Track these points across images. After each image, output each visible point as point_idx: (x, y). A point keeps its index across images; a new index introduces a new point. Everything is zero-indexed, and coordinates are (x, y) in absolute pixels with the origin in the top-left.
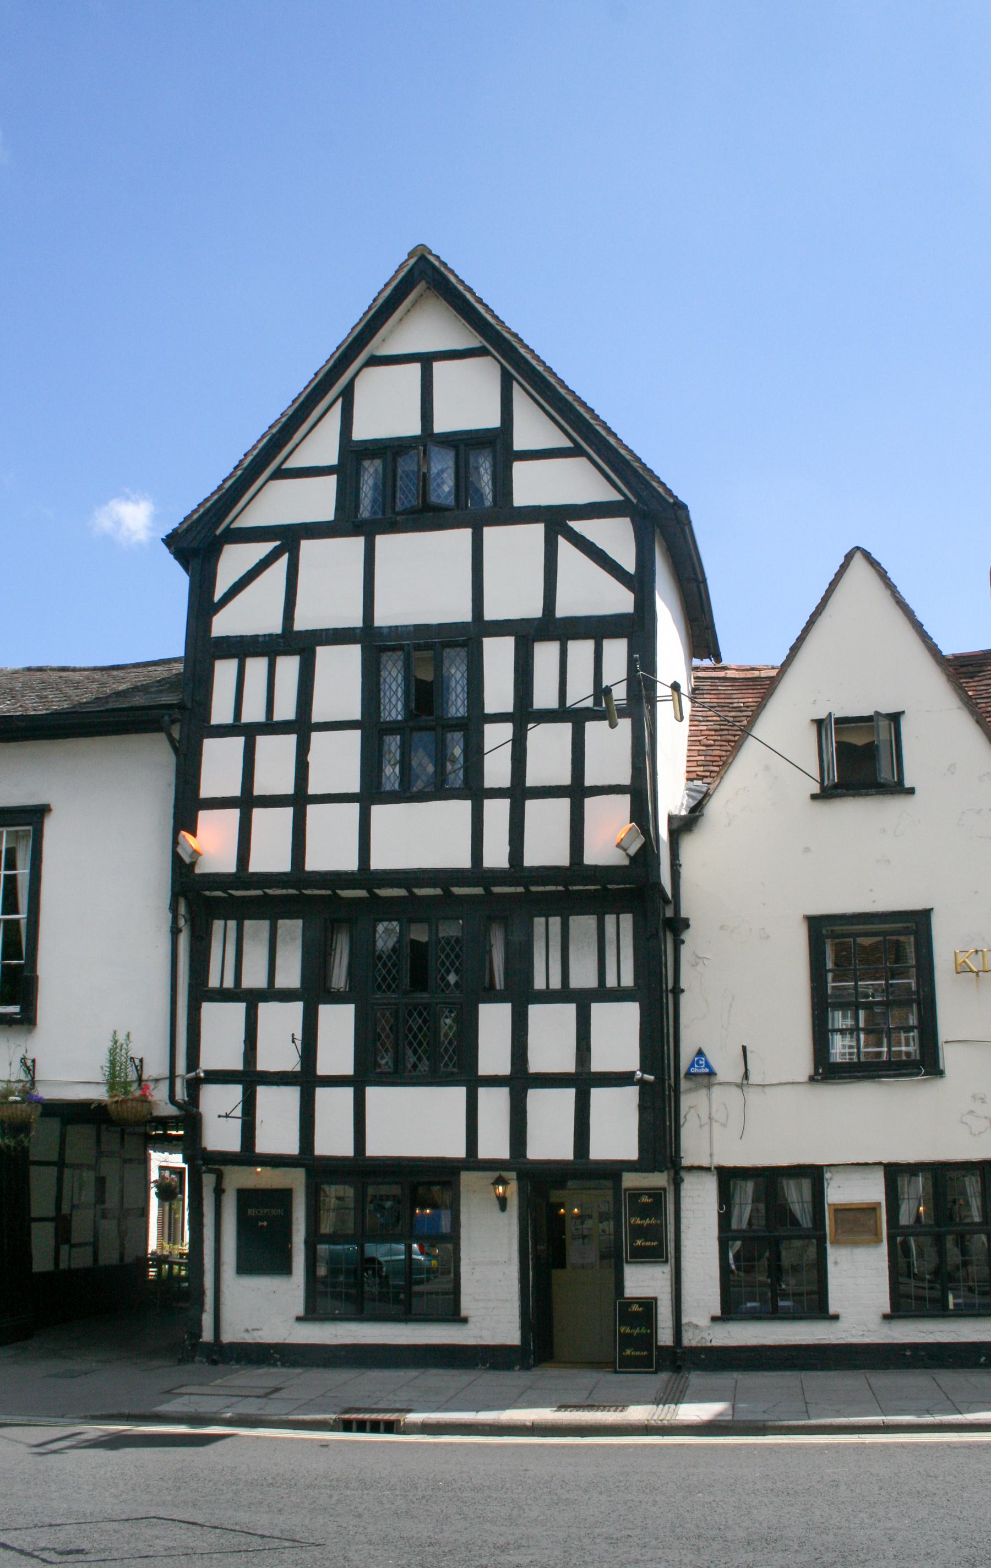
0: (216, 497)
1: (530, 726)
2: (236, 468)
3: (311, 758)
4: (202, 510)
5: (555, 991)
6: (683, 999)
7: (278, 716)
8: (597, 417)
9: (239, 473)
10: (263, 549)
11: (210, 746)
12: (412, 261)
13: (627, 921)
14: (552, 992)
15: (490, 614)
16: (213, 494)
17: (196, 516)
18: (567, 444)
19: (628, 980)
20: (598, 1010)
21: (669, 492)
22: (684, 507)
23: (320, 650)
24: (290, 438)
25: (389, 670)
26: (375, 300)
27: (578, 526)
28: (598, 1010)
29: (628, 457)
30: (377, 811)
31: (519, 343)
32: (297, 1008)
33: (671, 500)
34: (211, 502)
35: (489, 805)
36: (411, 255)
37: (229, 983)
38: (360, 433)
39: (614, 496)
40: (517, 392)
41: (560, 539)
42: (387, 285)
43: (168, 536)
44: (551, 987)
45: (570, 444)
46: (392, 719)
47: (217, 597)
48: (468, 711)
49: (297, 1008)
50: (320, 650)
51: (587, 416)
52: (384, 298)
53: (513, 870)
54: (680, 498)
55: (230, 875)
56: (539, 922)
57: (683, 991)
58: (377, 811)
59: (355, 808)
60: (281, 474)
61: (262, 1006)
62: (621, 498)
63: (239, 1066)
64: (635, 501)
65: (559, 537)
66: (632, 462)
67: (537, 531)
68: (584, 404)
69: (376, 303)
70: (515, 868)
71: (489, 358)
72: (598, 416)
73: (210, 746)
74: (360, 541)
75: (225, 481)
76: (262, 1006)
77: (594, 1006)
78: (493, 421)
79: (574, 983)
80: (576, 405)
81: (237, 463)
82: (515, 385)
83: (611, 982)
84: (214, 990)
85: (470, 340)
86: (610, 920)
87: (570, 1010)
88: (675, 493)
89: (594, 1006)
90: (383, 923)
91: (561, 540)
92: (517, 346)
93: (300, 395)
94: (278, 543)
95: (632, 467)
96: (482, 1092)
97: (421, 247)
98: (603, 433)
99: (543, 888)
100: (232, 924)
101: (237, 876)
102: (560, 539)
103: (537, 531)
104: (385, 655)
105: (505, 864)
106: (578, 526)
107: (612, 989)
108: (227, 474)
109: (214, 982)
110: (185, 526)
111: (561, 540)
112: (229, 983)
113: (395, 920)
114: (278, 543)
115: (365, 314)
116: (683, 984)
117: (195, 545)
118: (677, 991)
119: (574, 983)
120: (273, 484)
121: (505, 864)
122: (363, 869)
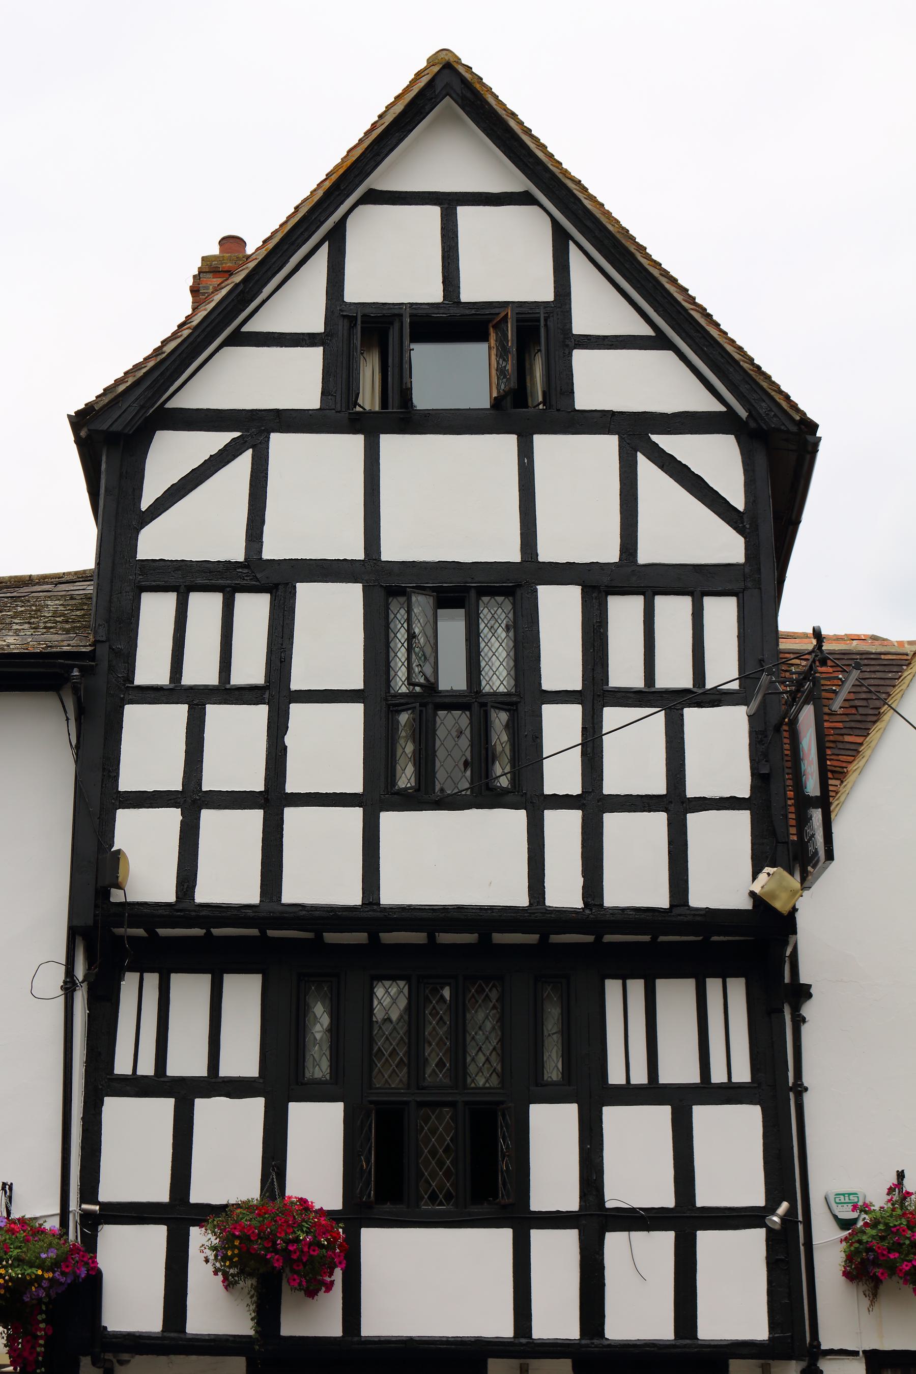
0: (151, 364)
1: (508, 713)
2: (181, 326)
3: (289, 740)
4: (130, 381)
5: (741, 1086)
6: (807, 1098)
7: (239, 678)
8: (692, 300)
9: (186, 333)
10: (219, 440)
11: (133, 714)
12: (436, 69)
13: (738, 989)
14: (224, 1082)
15: (546, 553)
16: (146, 359)
17: (122, 388)
18: (645, 330)
19: (742, 1074)
20: (702, 1115)
21: (794, 406)
22: (814, 427)
23: (302, 589)
24: (259, 292)
25: (402, 623)
26: (381, 117)
27: (666, 442)
28: (702, 1115)
29: (737, 357)
30: (388, 820)
31: (582, 193)
32: (256, 1106)
33: (798, 418)
34: (144, 370)
35: (553, 819)
36: (431, 61)
37: (147, 1068)
38: (354, 292)
39: (712, 405)
40: (576, 259)
41: (641, 458)
42: (398, 98)
43: (78, 413)
44: (634, 1081)
45: (648, 331)
46: (492, 691)
47: (145, 505)
48: (516, 685)
49: (256, 1106)
50: (302, 589)
51: (679, 297)
52: (394, 116)
53: (588, 912)
54: (809, 415)
55: (168, 905)
56: (613, 988)
57: (806, 1089)
58: (388, 820)
59: (356, 815)
60: (241, 339)
61: (200, 1104)
62: (723, 409)
63: (162, 1194)
64: (743, 413)
65: (639, 454)
66: (741, 363)
67: (609, 444)
68: (674, 281)
69: (382, 121)
70: (591, 910)
71: (535, 209)
72: (694, 299)
73: (133, 714)
74: (358, 441)
75: (165, 342)
76: (200, 1104)
77: (199, 1103)
78: (546, 293)
79: (174, 1069)
80: (663, 281)
81: (183, 319)
82: (572, 247)
83: (718, 1076)
84: (123, 1078)
85: (515, 181)
86: (713, 986)
87: (165, 1107)
88: (801, 406)
89: (199, 1103)
90: (398, 982)
91: (641, 459)
92: (581, 196)
93: (274, 233)
94: (238, 434)
95: (741, 367)
96: (538, 1237)
97: (444, 52)
98: (702, 321)
99: (718, 937)
100: (636, 988)
101: (177, 907)
102: (641, 458)
103: (609, 444)
104: (395, 600)
105: (578, 904)
106: (666, 442)
107: (720, 1086)
108: (168, 334)
109: (122, 1066)
110: (106, 400)
111: (641, 459)
112: (147, 1068)
113: (401, 978)
114: (238, 434)
115: (367, 134)
116: (806, 1080)
117: (117, 427)
118: (800, 1090)
119: (174, 1069)
120: (228, 351)
121: (578, 904)
122: (370, 904)
